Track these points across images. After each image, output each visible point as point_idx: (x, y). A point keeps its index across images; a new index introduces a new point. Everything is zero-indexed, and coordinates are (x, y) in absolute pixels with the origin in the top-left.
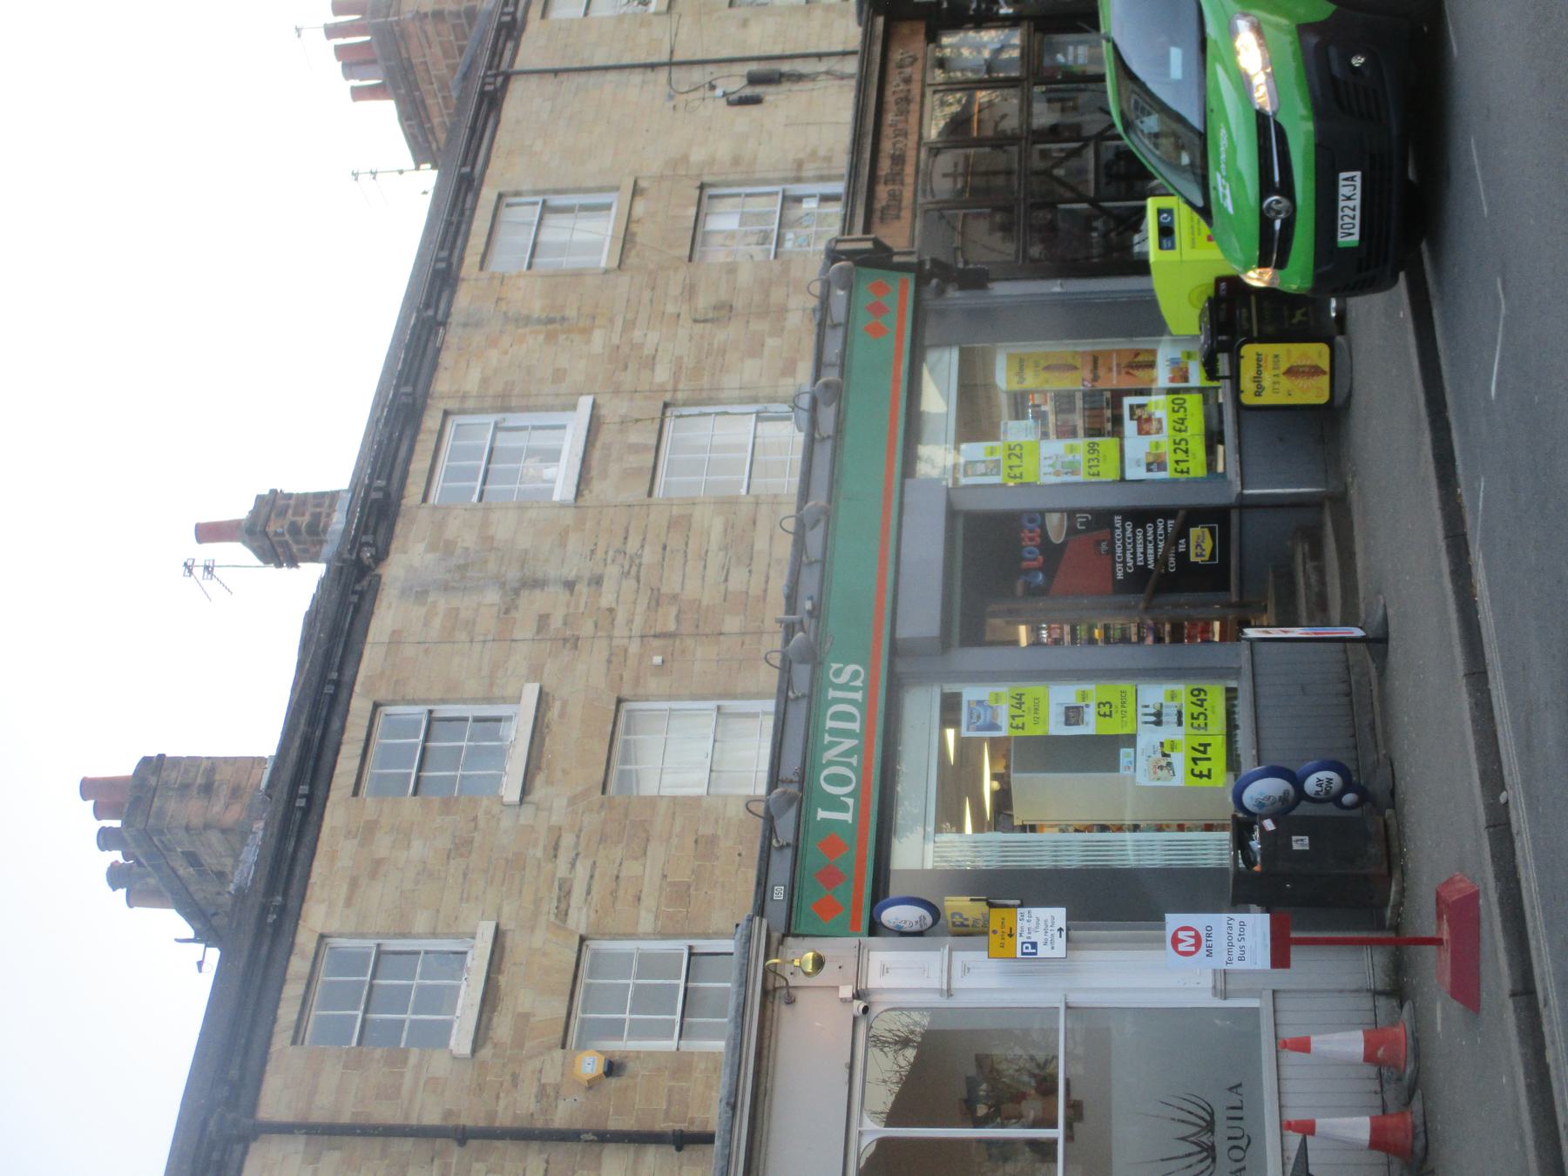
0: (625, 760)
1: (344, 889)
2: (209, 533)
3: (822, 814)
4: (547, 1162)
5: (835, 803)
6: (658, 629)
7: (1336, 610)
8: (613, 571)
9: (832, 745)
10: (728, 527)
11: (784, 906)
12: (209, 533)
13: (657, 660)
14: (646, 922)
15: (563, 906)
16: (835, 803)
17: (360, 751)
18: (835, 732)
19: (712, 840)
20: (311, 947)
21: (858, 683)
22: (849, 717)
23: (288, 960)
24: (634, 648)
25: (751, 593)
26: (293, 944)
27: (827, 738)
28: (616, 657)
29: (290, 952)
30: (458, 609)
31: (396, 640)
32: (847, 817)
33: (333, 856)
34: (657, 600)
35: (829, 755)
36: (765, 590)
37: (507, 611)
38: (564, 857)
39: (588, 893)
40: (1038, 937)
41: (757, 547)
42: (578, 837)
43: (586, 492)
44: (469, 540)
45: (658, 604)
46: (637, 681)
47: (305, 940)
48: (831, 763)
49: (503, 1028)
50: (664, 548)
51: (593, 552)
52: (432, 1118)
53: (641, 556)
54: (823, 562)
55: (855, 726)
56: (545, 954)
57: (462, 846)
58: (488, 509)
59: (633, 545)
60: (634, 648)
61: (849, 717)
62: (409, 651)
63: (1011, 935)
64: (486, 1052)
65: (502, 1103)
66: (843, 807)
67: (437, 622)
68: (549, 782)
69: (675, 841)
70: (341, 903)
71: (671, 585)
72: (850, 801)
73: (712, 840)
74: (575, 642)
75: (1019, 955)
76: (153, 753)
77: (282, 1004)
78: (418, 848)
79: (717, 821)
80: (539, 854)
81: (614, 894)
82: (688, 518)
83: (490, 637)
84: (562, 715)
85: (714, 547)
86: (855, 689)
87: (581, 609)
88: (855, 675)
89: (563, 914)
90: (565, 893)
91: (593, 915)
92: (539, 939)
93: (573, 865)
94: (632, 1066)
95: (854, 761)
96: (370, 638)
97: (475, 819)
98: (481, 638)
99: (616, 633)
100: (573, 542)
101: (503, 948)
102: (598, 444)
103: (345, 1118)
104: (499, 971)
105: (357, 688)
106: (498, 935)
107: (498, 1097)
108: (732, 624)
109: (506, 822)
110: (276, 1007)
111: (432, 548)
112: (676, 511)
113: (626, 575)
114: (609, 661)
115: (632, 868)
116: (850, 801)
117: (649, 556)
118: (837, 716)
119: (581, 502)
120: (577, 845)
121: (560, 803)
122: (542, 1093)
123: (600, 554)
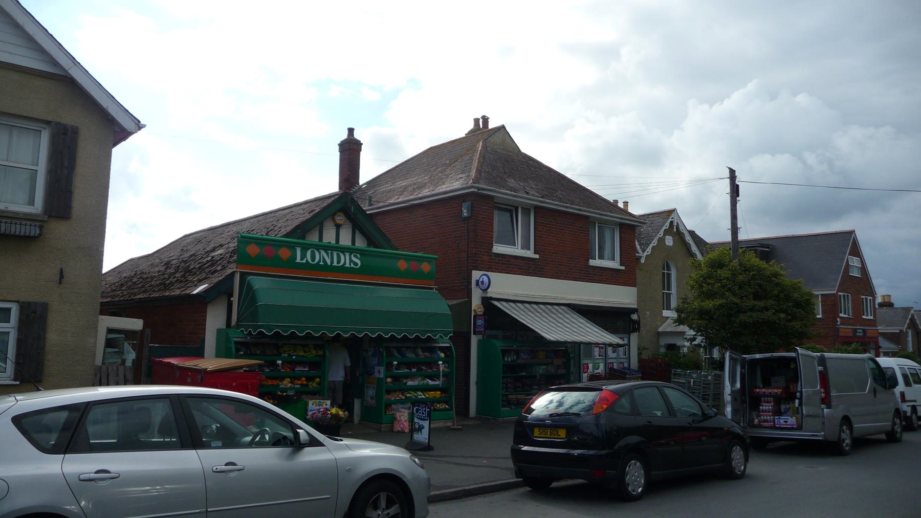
2: (351, 131)
5: (303, 256)
7: (519, 241)
9: (324, 261)
12: (351, 131)
16: (303, 256)
22: (339, 262)
32: (298, 260)
48: (320, 253)
55: (335, 264)
61: (339, 262)
66: (302, 259)
72: (304, 261)
88: (356, 264)
95: (321, 263)
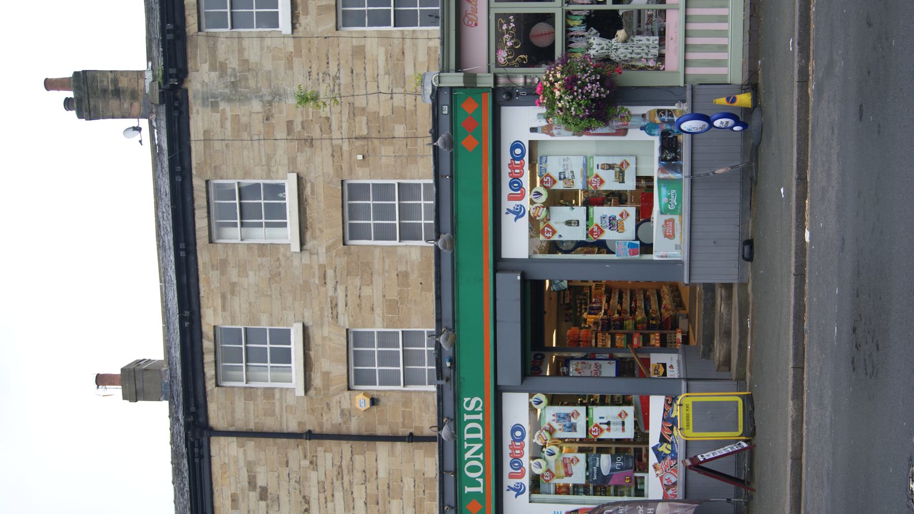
1: (219, 300)
3: (468, 490)
6: (357, 134)
9: (469, 448)
10: (389, 56)
11: (441, 103)
13: (360, 157)
14: (377, 252)
15: (335, 313)
17: (206, 215)
18: (470, 441)
19: (406, 275)
20: (211, 334)
21: (479, 409)
22: (476, 431)
23: (202, 342)
25: (407, 107)
26: (201, 332)
27: (466, 445)
28: (336, 153)
29: (202, 354)
31: (207, 139)
32: (480, 489)
33: (208, 282)
34: (354, 112)
35: (468, 455)
41: (407, 73)
43: (297, 25)
46: (351, 170)
47: (207, 330)
48: (469, 459)
49: (317, 380)
52: (293, 427)
53: (338, 78)
54: (453, 329)
55: (480, 436)
56: (330, 340)
57: (274, 277)
59: (333, 70)
60: (346, 147)
61: (476, 431)
62: (217, 145)
64: (312, 392)
65: (325, 417)
66: (478, 485)
67: (228, 124)
68: (314, 238)
70: (220, 308)
71: (360, 102)
72: (481, 480)
73: (406, 275)
74: (310, 141)
76: (80, 69)
77: (205, 366)
78: (252, 277)
79: (406, 263)
80: (317, 282)
81: (359, 305)
83: (262, 137)
84: (313, 192)
85: (381, 72)
86: (478, 413)
87: (310, 118)
88: (478, 404)
90: (334, 306)
91: (351, 319)
92: (326, 331)
93: (336, 289)
94: (383, 400)
96: (193, 137)
98: (256, 137)
100: (296, 62)
101: (309, 336)
103: (252, 427)
104: (309, 350)
105: (194, 172)
106: (305, 329)
108: (400, 130)
109: (296, 262)
110: (203, 368)
111: (213, 68)
115: (367, 291)
116: (481, 480)
117: (344, 79)
118: (471, 431)
119: (296, 35)
120: (336, 276)
121: (322, 250)
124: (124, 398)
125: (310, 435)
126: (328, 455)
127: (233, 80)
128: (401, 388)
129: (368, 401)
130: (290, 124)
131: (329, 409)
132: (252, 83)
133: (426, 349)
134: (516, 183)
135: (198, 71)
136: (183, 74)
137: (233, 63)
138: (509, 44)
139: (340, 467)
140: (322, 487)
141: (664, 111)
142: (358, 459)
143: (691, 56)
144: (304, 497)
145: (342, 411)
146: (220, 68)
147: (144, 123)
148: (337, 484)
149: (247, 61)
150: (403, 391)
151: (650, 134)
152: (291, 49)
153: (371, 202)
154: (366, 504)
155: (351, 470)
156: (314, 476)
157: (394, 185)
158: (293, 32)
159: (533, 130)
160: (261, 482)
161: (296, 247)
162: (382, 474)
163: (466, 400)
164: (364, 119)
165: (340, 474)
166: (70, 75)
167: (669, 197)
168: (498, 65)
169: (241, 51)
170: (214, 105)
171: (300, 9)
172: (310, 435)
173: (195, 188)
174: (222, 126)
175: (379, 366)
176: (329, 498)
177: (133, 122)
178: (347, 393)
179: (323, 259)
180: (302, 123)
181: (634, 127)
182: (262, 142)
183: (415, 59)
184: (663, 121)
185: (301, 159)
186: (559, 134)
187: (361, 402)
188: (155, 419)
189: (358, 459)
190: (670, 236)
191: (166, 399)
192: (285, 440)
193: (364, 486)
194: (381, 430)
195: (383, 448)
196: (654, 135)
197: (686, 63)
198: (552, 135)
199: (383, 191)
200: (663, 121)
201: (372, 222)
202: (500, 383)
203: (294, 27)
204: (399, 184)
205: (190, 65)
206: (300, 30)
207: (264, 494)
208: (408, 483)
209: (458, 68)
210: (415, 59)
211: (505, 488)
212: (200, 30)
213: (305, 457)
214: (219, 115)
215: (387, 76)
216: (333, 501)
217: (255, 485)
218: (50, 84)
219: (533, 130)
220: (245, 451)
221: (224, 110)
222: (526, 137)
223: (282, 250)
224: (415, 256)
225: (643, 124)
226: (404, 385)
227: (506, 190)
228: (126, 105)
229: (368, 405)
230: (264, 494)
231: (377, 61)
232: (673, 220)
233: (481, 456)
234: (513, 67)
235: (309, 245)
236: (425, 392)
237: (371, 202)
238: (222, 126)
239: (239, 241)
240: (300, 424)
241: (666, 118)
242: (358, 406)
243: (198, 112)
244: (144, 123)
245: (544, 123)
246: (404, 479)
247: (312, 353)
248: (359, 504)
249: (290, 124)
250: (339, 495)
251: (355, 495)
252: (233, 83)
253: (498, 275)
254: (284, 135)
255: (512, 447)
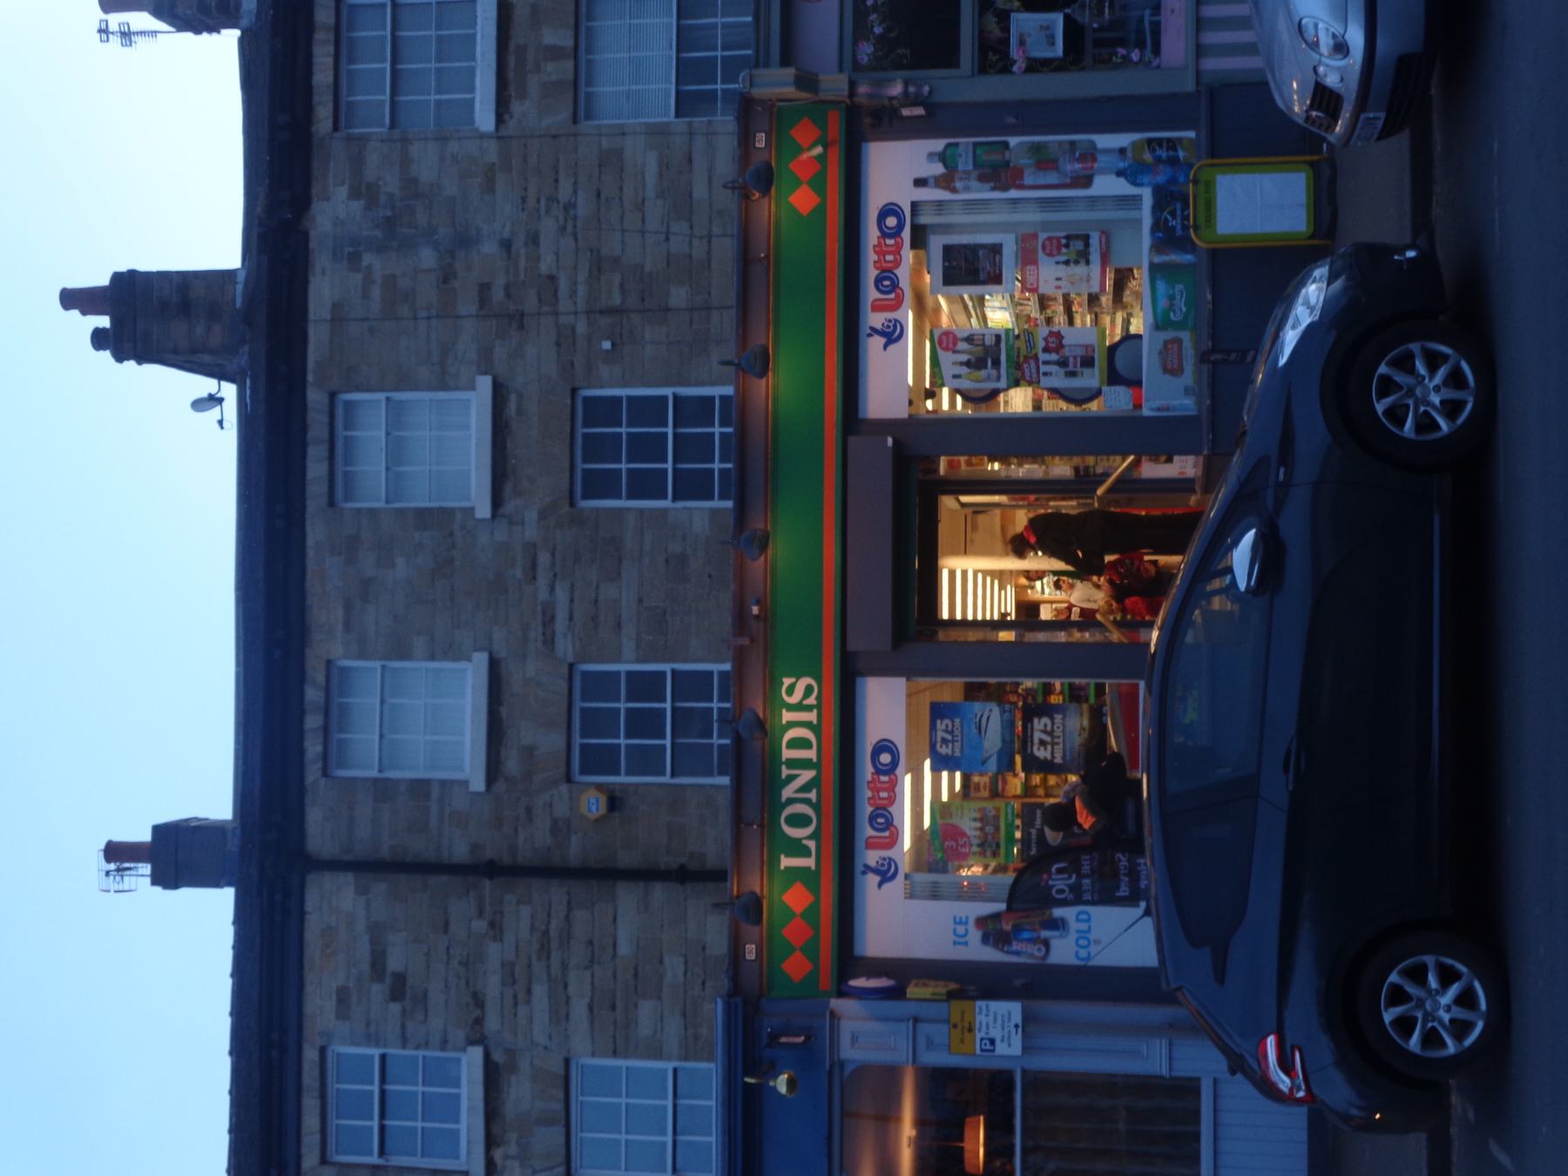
0: (589, 83)
1: (340, 613)
4: (569, 894)
8: (548, 226)
9: (791, 778)
10: (664, 166)
13: (607, 345)
17: (326, 454)
18: (792, 763)
21: (812, 700)
24: (581, 328)
27: (785, 772)
28: (565, 339)
30: (394, 276)
31: (338, 317)
32: (810, 862)
34: (599, 265)
35: (788, 792)
36: (709, 253)
37: (446, 280)
38: (543, 581)
39: (571, 619)
40: (995, 1033)
41: (695, 195)
42: (553, 555)
43: (506, 117)
44: (391, 184)
45: (599, 270)
48: (791, 801)
49: (512, 763)
50: (599, 195)
51: (524, 199)
52: (460, 851)
53: (574, 206)
58: (405, 140)
60: (581, 328)
63: (970, 1030)
64: (500, 786)
65: (521, 837)
66: (805, 852)
67: (376, 292)
69: (647, 560)
70: (340, 627)
72: (812, 844)
75: (978, 1051)
76: (123, 268)
78: (401, 568)
80: (519, 573)
81: (594, 618)
82: (618, 153)
83: (434, 312)
84: (520, 411)
85: (650, 192)
86: (809, 708)
89: (549, 641)
90: (549, 620)
92: (531, 669)
93: (552, 589)
96: (311, 316)
97: (451, 534)
98: (424, 314)
99: (562, 309)
102: (512, 46)
103: (385, 853)
105: (310, 378)
107: (516, 830)
108: (678, 296)
111: (354, 194)
112: (605, 143)
113: (563, 229)
114: (558, 344)
116: (812, 844)
117: (583, 209)
119: (503, 133)
120: (553, 564)
121: (531, 516)
122: (555, 827)
123: (531, 201)
124: (154, 883)
125: (491, 869)
126: (523, 914)
127: (389, 213)
128: (666, 779)
129: (603, 800)
130: (484, 289)
131: (531, 820)
132: (421, 218)
133: (715, 705)
134: (888, 281)
135: (328, 199)
136: (302, 203)
137: (391, 184)
138: (877, 30)
139: (546, 933)
140: (509, 973)
141: (1159, 142)
142: (580, 915)
143: (1211, 37)
144: (475, 995)
145: (555, 822)
146: (364, 191)
147: (229, 391)
148: (538, 967)
149: (415, 181)
150: (669, 785)
151: (1134, 183)
152: (493, 157)
153: (623, 430)
154: (591, 1009)
155: (566, 937)
156: (494, 951)
157: (664, 673)
158: (497, 128)
159: (920, 183)
160: (394, 963)
161: (484, 511)
162: (624, 948)
163: (787, 681)
164: (617, 279)
165: (545, 949)
166: (104, 281)
167: (1171, 298)
168: (857, 66)
169: (406, 162)
170: (354, 260)
171: (512, 90)
172: (491, 869)
173: (315, 90)
174: (366, 296)
175: (628, 736)
176: (521, 996)
177: (205, 385)
178: (564, 788)
179: (531, 533)
180: (507, 287)
181: (1104, 171)
182: (434, 322)
183: (711, 170)
184: (1158, 160)
185: (500, 352)
186: (967, 189)
187: (593, 805)
188: (209, 915)
189: (580, 915)
190: (1174, 370)
191: (229, 884)
192: (444, 878)
193: (588, 973)
194: (626, 859)
195: (627, 897)
196: (1141, 185)
197: (1200, 51)
198: (954, 190)
199: (649, 410)
200: (1158, 160)
201: (623, 466)
202: (851, 647)
203: (500, 120)
204: (674, 672)
205: (316, 189)
206: (511, 127)
207: (399, 987)
208: (673, 967)
209: (786, 61)
210: (711, 170)
211: (865, 330)
212: (336, 127)
213: (481, 914)
214: (360, 276)
215: (659, 202)
216: (528, 1002)
217: (384, 970)
218: (73, 299)
219: (920, 183)
220: (368, 903)
221: (369, 267)
222: (905, 196)
223: (459, 516)
224: (700, 526)
225: (1121, 165)
226: (673, 775)
227: (871, 294)
228: (200, 330)
229: (603, 810)
230: (399, 987)
231: (643, 174)
232: (1179, 341)
233: (813, 795)
234: (884, 69)
235: (510, 507)
236: (712, 786)
237: (623, 430)
238: (366, 296)
239: (381, 504)
240: (475, 847)
241: (1163, 154)
242: (584, 809)
243: (323, 273)
244: (229, 391)
245: (938, 169)
246: (667, 960)
247: (504, 711)
248: (579, 1010)
249: (484, 289)
250: (540, 991)
251: (572, 990)
252: (388, 219)
253: (852, 439)
254: (473, 309)
255: (880, 251)
